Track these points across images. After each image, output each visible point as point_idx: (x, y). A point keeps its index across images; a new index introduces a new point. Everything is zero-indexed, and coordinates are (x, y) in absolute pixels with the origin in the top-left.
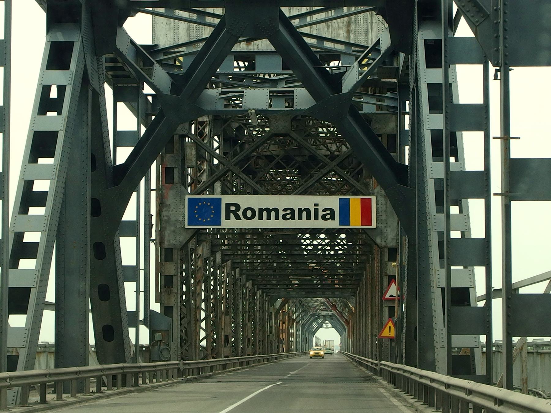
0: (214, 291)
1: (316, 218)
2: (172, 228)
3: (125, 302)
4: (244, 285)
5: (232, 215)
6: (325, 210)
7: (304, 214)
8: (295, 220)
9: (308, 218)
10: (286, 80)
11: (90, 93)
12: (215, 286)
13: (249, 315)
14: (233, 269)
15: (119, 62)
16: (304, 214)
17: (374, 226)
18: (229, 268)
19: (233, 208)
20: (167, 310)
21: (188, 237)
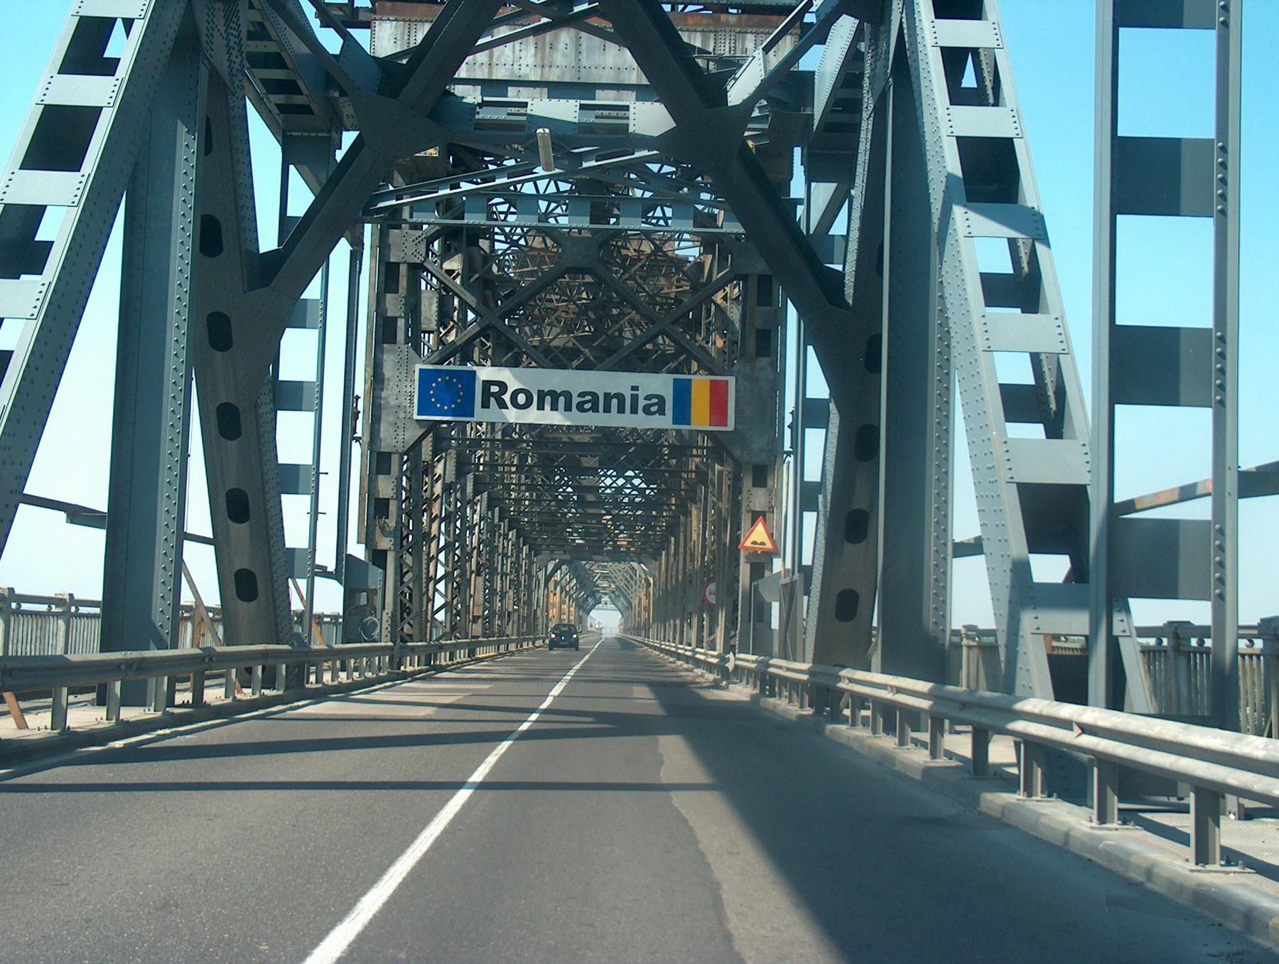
0: (461, 538)
1: (634, 410)
2: (392, 418)
3: (283, 528)
4: (506, 536)
5: (492, 399)
6: (648, 398)
7: (614, 402)
8: (598, 412)
9: (621, 410)
10: (596, 154)
11: (204, 73)
12: (463, 529)
13: (510, 580)
14: (490, 507)
15: (272, 40)
16: (614, 402)
17: (731, 426)
18: (484, 505)
19: (495, 389)
20: (378, 557)
21: (420, 432)
